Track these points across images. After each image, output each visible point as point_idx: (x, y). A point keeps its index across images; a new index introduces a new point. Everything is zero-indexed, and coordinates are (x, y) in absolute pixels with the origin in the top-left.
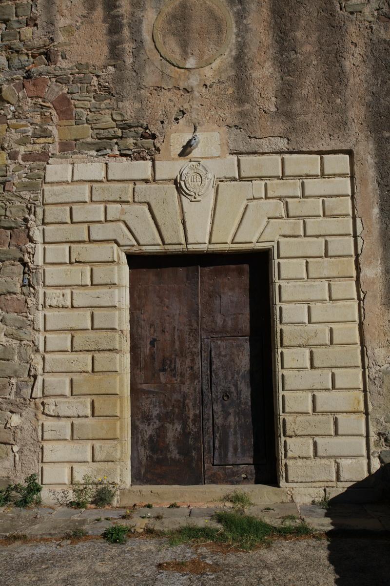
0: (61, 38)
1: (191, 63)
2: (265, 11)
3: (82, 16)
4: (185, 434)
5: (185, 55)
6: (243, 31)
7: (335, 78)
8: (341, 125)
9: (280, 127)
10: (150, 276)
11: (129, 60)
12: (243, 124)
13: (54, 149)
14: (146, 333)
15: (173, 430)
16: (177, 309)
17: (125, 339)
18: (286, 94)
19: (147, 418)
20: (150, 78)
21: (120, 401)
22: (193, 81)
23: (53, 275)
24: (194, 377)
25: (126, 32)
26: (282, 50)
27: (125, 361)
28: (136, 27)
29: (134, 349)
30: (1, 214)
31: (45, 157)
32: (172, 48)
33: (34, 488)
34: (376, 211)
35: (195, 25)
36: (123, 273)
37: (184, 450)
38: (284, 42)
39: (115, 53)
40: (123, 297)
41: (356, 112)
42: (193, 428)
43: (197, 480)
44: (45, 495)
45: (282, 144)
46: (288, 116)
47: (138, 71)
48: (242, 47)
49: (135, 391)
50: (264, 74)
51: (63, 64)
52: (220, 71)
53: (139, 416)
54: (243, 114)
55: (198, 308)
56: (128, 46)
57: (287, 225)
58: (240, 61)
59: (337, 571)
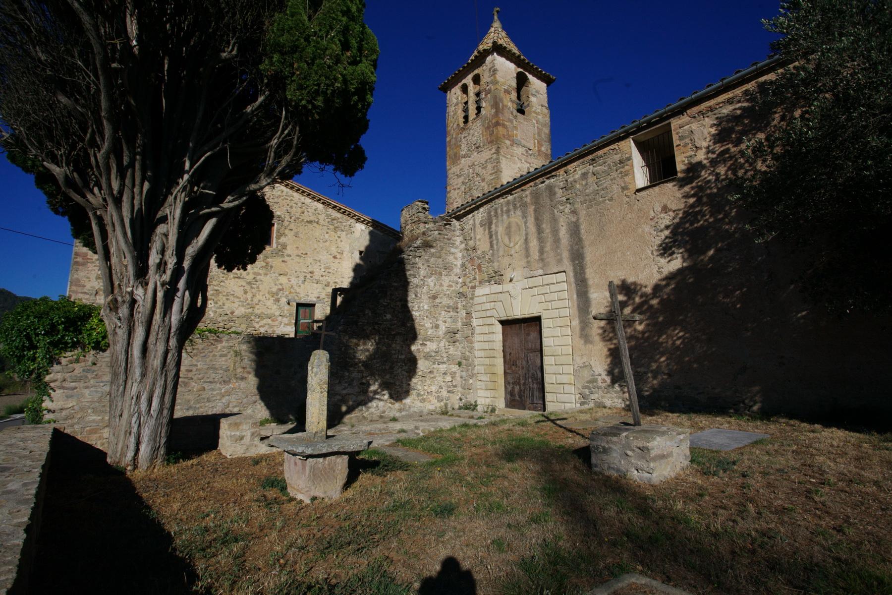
0: (478, 243)
4: (520, 390)
6: (527, 227)
7: (557, 241)
8: (560, 261)
9: (540, 265)
10: (508, 328)
12: (528, 265)
13: (477, 284)
14: (508, 350)
15: (517, 388)
16: (516, 340)
18: (542, 251)
19: (509, 383)
22: (513, 252)
23: (478, 330)
24: (523, 368)
26: (539, 234)
27: (500, 361)
28: (496, 233)
29: (504, 357)
30: (2, 468)
31: (474, 287)
32: (506, 240)
33: (476, 406)
34: (575, 296)
36: (499, 328)
37: (520, 397)
38: (540, 231)
39: (492, 246)
40: (499, 337)
41: (566, 255)
42: (522, 388)
43: (523, 408)
44: (478, 408)
45: (541, 272)
46: (542, 260)
47: (498, 250)
48: (527, 235)
49: (505, 373)
50: (534, 244)
51: (479, 252)
53: (507, 383)
54: (528, 262)
56: (495, 242)
57: (544, 306)
58: (526, 241)
59: (72, 225)
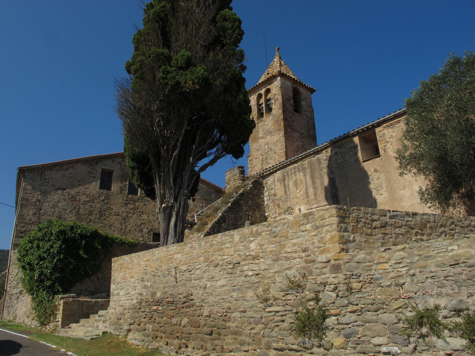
1: (298, 191)
2: (310, 177)
3: (199, 7)
5: (297, 190)
6: (306, 181)
9: (315, 202)
11: (288, 193)
17: (128, 298)
18: (315, 194)
20: (292, 196)
21: (311, 172)
22: (299, 195)
25: (287, 187)
26: (314, 185)
35: (298, 183)
38: (314, 183)
46: (316, 199)
47: (290, 195)
51: (278, 197)
52: (303, 192)
54: (308, 201)
55: (350, 202)
56: (288, 190)
